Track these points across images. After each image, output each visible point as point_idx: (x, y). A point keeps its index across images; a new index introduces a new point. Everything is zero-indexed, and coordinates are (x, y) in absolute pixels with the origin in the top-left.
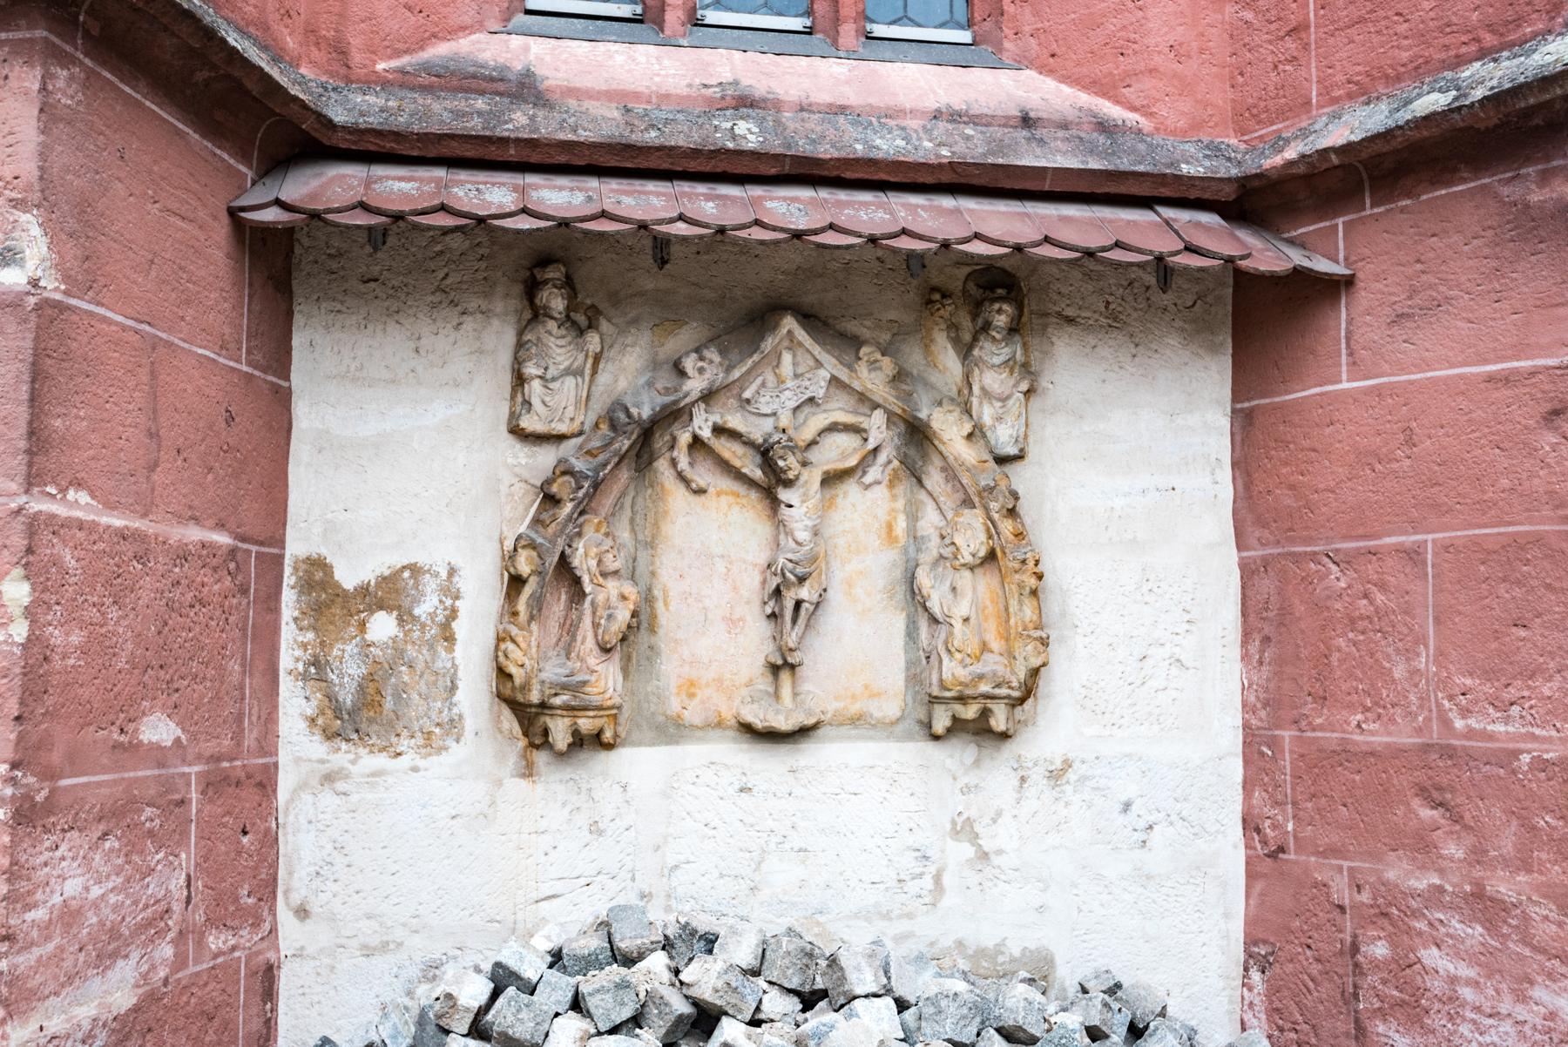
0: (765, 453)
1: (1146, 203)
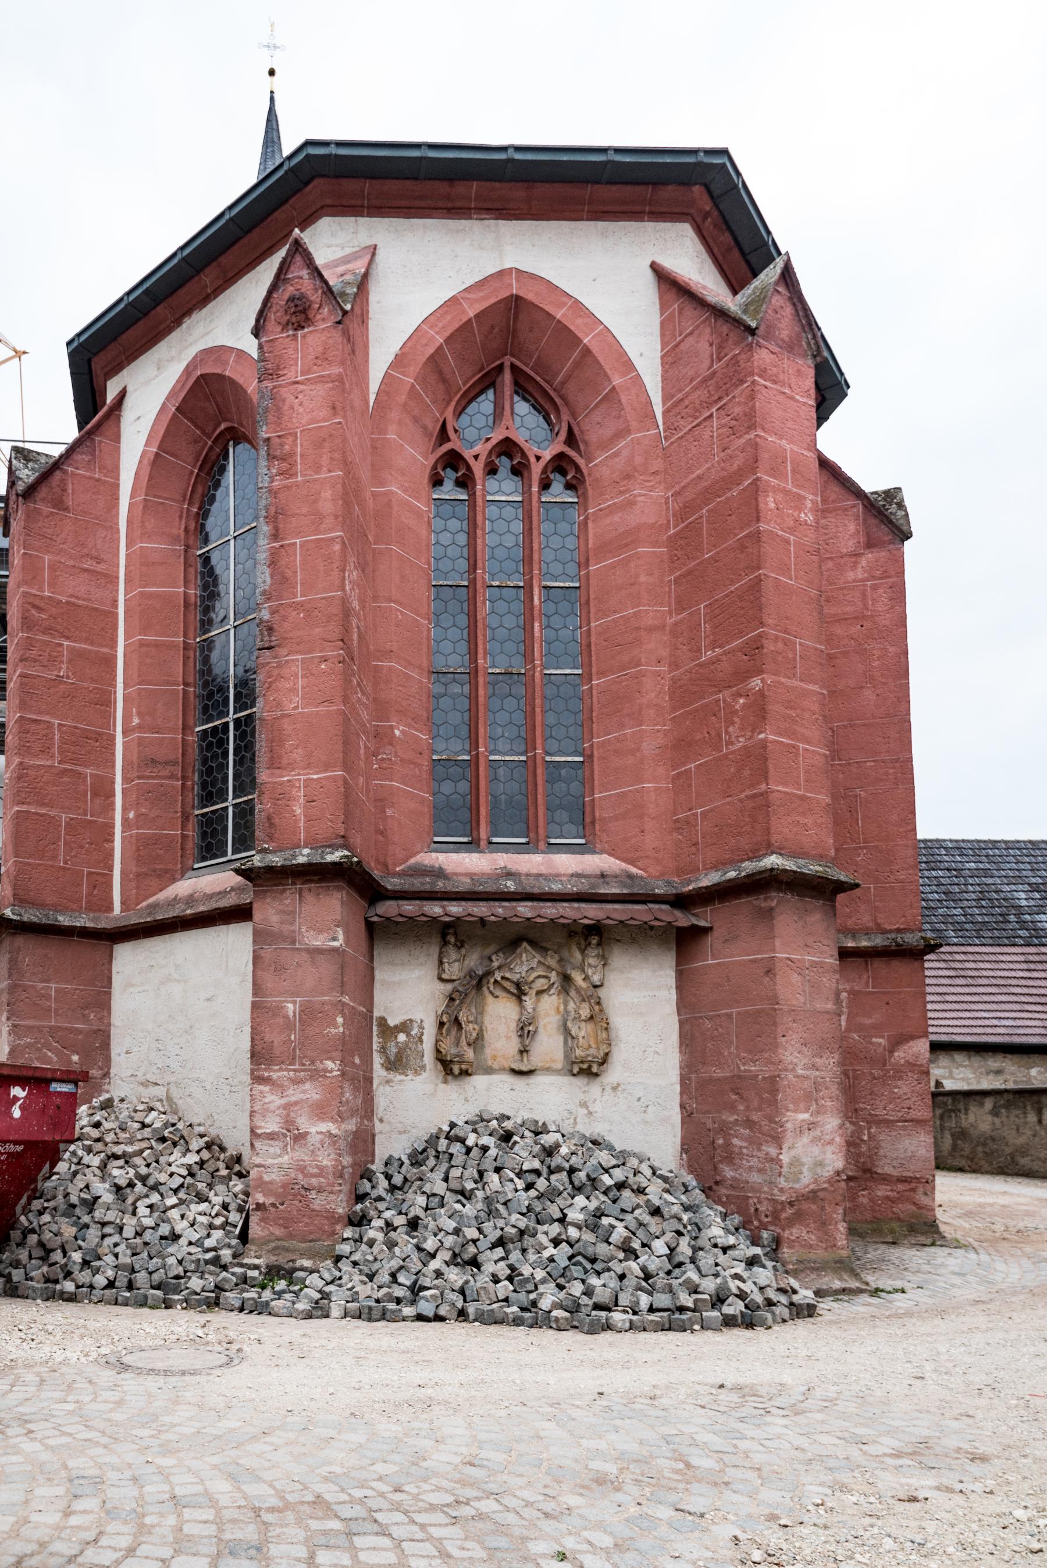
0: (518, 985)
1: (644, 902)
